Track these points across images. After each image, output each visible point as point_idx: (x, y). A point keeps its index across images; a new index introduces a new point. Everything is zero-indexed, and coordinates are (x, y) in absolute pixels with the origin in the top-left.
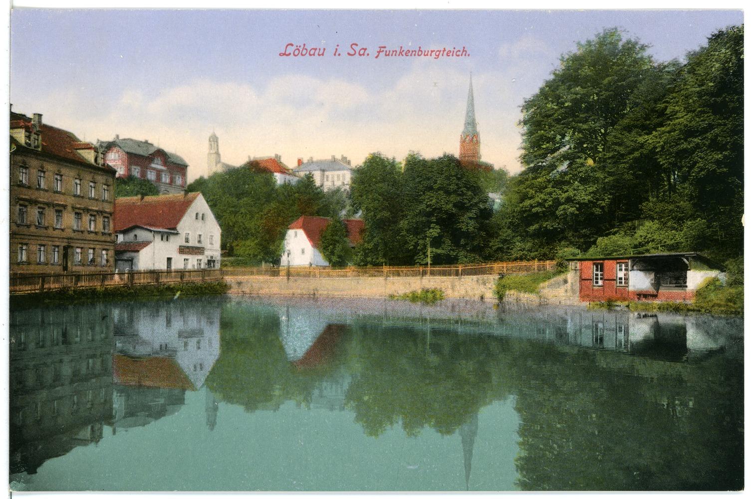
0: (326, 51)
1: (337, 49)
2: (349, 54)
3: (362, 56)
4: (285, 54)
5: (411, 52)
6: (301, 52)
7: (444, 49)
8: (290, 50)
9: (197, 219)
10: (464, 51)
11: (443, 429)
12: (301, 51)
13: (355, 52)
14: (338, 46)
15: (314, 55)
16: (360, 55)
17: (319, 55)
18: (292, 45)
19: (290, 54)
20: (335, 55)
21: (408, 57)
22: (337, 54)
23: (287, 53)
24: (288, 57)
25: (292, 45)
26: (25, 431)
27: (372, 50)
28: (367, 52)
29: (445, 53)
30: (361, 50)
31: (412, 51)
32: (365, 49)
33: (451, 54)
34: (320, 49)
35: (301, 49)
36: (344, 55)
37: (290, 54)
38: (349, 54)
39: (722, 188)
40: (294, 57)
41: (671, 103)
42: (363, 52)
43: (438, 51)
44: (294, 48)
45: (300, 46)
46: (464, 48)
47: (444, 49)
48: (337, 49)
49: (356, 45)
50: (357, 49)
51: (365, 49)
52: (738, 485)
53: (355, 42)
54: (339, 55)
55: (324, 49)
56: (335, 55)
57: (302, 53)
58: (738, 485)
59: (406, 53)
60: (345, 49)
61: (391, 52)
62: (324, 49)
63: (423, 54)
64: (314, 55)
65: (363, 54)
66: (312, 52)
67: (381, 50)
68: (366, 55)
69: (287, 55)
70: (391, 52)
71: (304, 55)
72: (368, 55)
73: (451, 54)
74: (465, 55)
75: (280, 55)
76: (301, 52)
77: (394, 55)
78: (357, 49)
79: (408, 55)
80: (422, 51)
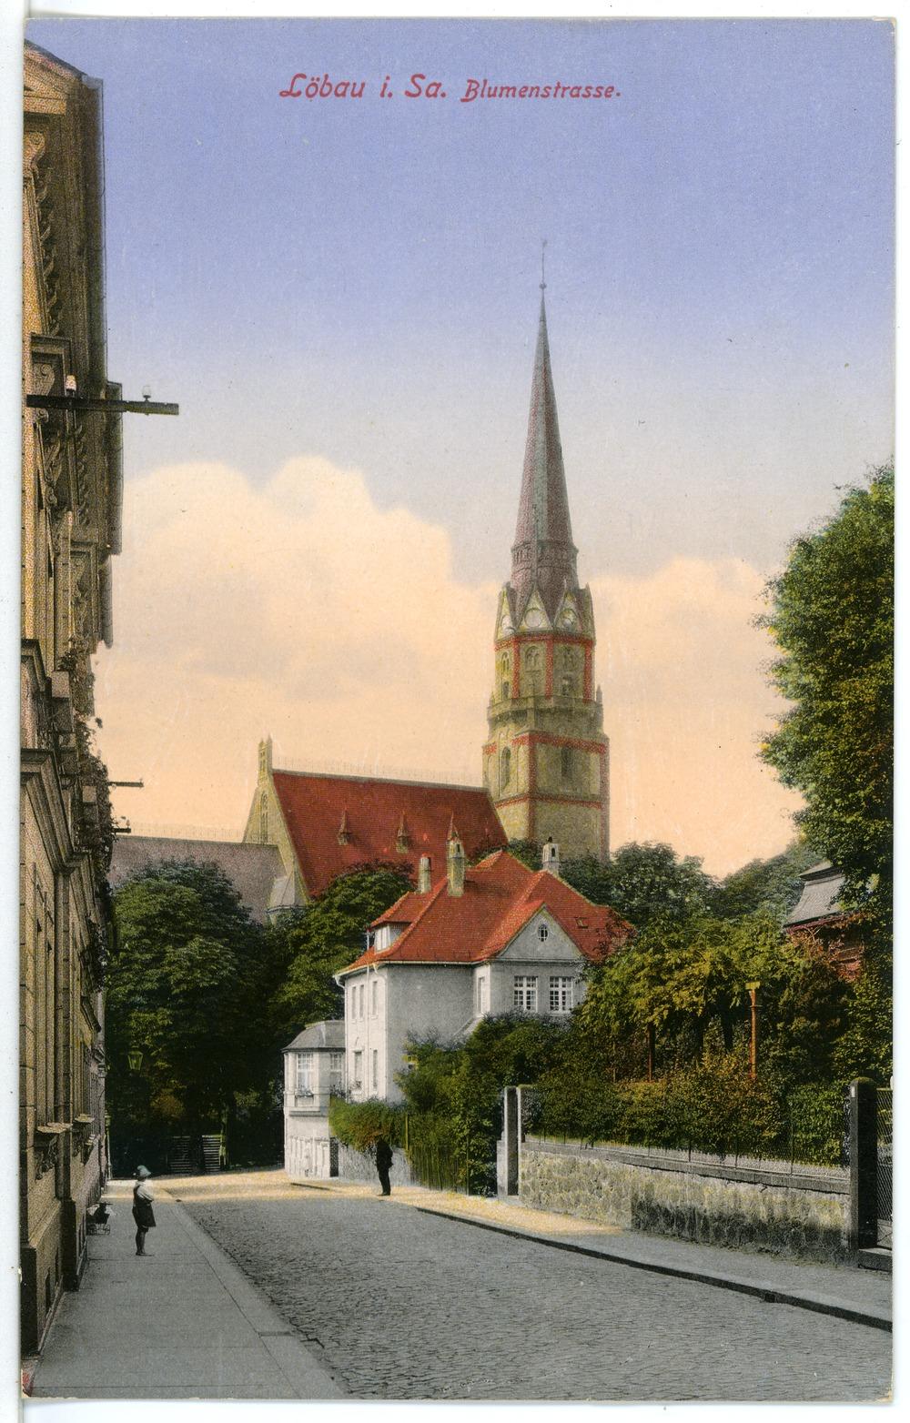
1: (473, 91)
2: (408, 94)
3: (432, 98)
4: (289, 93)
6: (319, 89)
7: (558, 83)
8: (301, 85)
9: (140, 785)
10: (325, 83)
12: (320, 88)
13: (420, 89)
14: (388, 78)
15: (343, 94)
18: (303, 76)
19: (299, 93)
20: (382, 95)
21: (524, 99)
22: (386, 93)
23: (295, 91)
24: (417, 98)
25: (303, 76)
27: (455, 86)
29: (560, 91)
30: (429, 87)
31: (533, 89)
32: (438, 85)
34: (355, 84)
35: (320, 84)
37: (299, 93)
38: (408, 94)
40: (426, 98)
42: (435, 91)
43: (343, 84)
44: (309, 81)
45: (318, 79)
47: (558, 83)
48: (385, 85)
49: (422, 77)
50: (423, 84)
51: (438, 85)
52: (874, 40)
53: (299, 72)
55: (363, 85)
56: (382, 95)
57: (336, 91)
58: (874, 40)
59: (607, 92)
60: (400, 85)
61: (499, 91)
62: (363, 85)
63: (334, 90)
64: (343, 94)
65: (435, 95)
66: (341, 90)
67: (473, 91)
68: (439, 94)
69: (294, 95)
70: (499, 91)
71: (327, 95)
72: (390, 95)
73: (528, 93)
74: (537, 96)
75: (281, 94)
76: (319, 89)
77: (534, 94)
78: (423, 84)
79: (524, 96)
80: (330, 84)
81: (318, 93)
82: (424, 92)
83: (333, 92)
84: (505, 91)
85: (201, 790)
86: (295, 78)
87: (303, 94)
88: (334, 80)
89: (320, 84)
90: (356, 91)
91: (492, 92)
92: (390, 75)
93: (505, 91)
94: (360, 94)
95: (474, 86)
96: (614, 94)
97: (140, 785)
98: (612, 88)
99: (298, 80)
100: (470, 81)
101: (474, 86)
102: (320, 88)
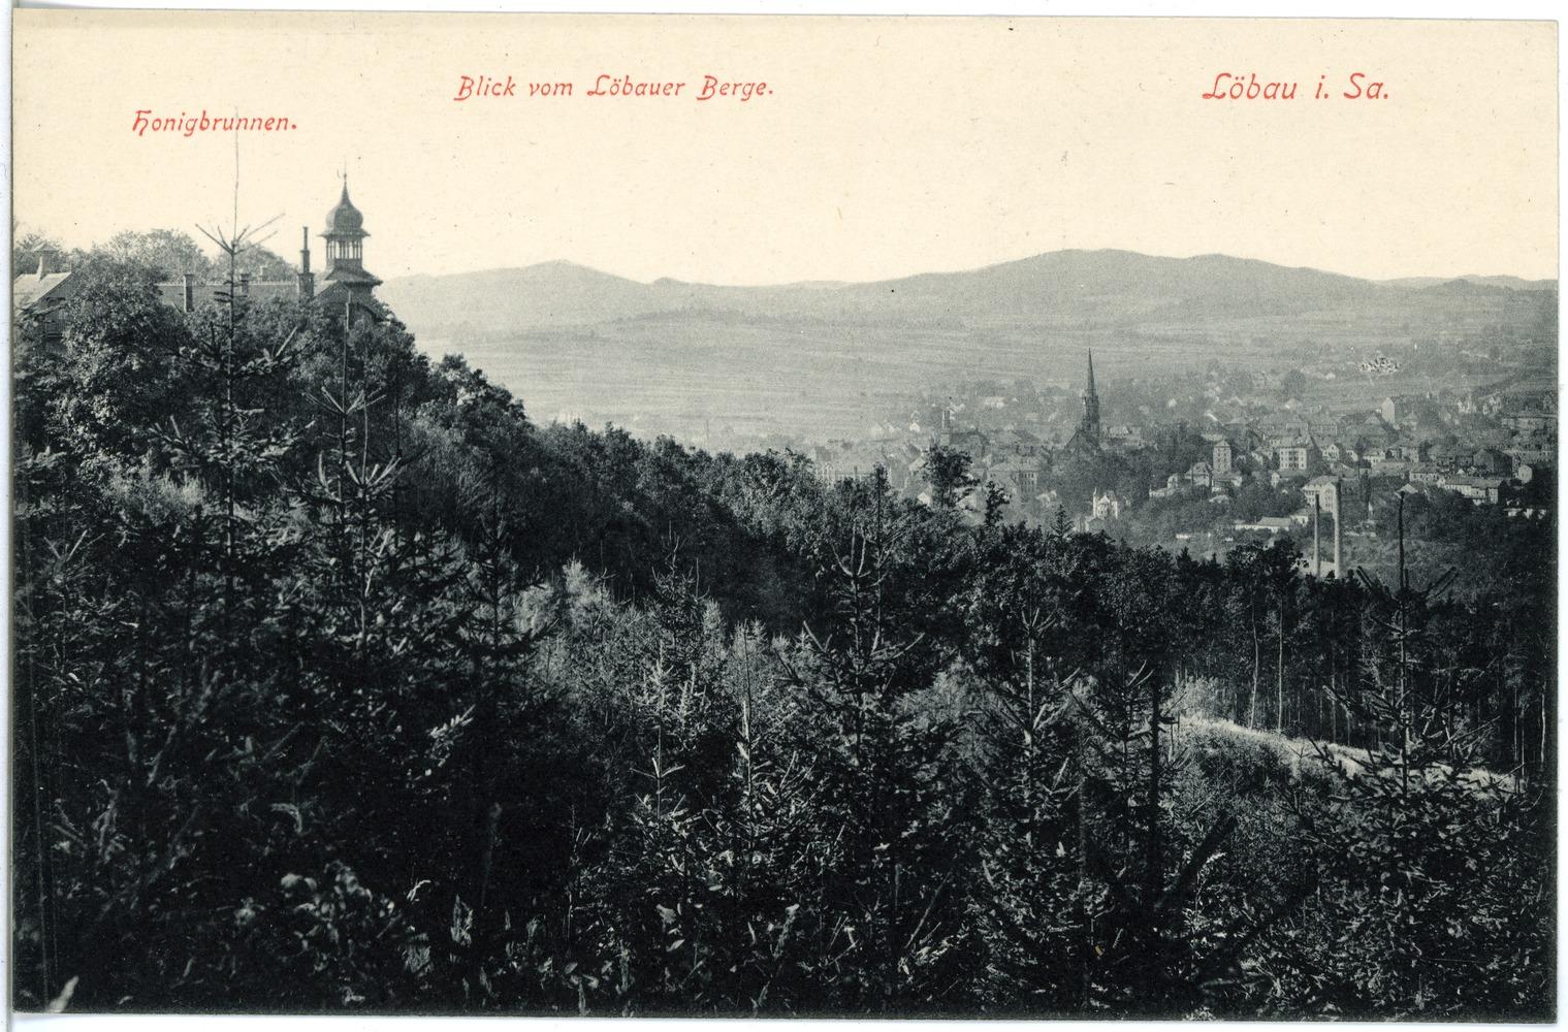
0: (559, 99)
1: (1321, 85)
2: (1346, 95)
5: (277, 122)
8: (1225, 85)
9: (306, 229)
11: (475, 565)
12: (1250, 89)
13: (1359, 89)
14: (1323, 77)
16: (1370, 96)
17: (1284, 97)
18: (1228, 75)
19: (1224, 95)
20: (1317, 97)
22: (1322, 95)
23: (1218, 93)
25: (1228, 75)
26: (1469, 320)
28: (1383, 91)
32: (1380, 85)
33: (274, 126)
35: (1246, 83)
36: (1337, 98)
37: (1224, 95)
38: (1346, 95)
39: (1427, 820)
41: (842, 651)
44: (1233, 81)
46: (204, 113)
48: (1321, 85)
50: (1363, 83)
52: (1543, 1010)
53: (1360, 71)
54: (1326, 96)
56: (1317, 97)
58: (1543, 1010)
60: (1338, 84)
63: (1245, 91)
64: (1274, 96)
65: (1377, 96)
66: (1270, 91)
67: (710, 86)
68: (1381, 95)
69: (1219, 97)
70: (235, 125)
73: (274, 126)
78: (1363, 83)
80: (207, 120)
81: (1262, 89)
82: (1364, 94)
83: (1262, 89)
84: (560, 88)
85: (715, 222)
86: (1220, 76)
87: (1228, 96)
88: (1262, 81)
89: (1246, 83)
90: (1288, 93)
91: (654, 90)
92: (1326, 72)
93: (560, 88)
94: (1292, 95)
95: (712, 82)
96: (766, 91)
97: (306, 229)
98: (765, 85)
99: (1224, 78)
100: (465, 78)
101: (468, 83)
102: (1250, 89)
